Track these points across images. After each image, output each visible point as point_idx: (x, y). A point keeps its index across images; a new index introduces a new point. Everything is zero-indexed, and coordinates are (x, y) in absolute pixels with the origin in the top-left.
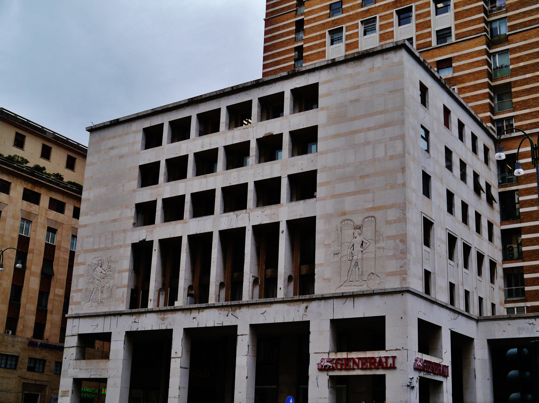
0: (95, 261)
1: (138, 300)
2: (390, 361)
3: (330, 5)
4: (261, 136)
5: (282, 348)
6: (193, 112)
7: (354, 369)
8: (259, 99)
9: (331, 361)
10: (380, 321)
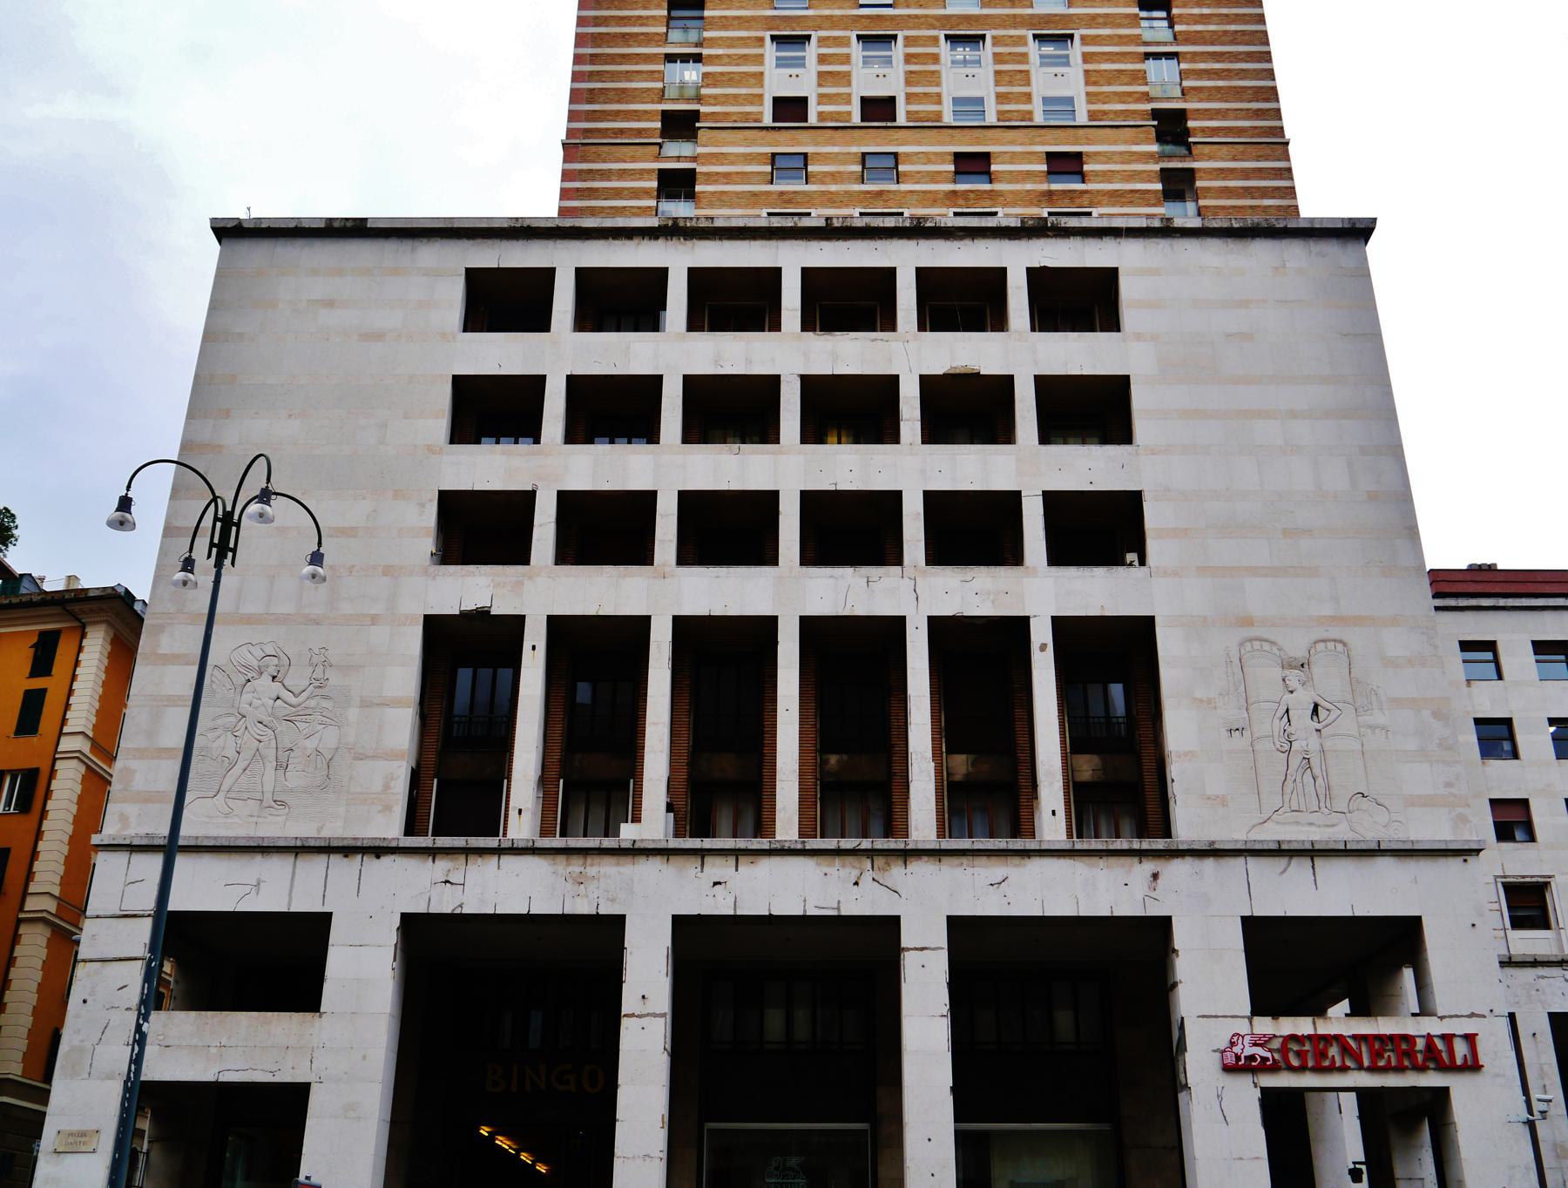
2: (1461, 1049)
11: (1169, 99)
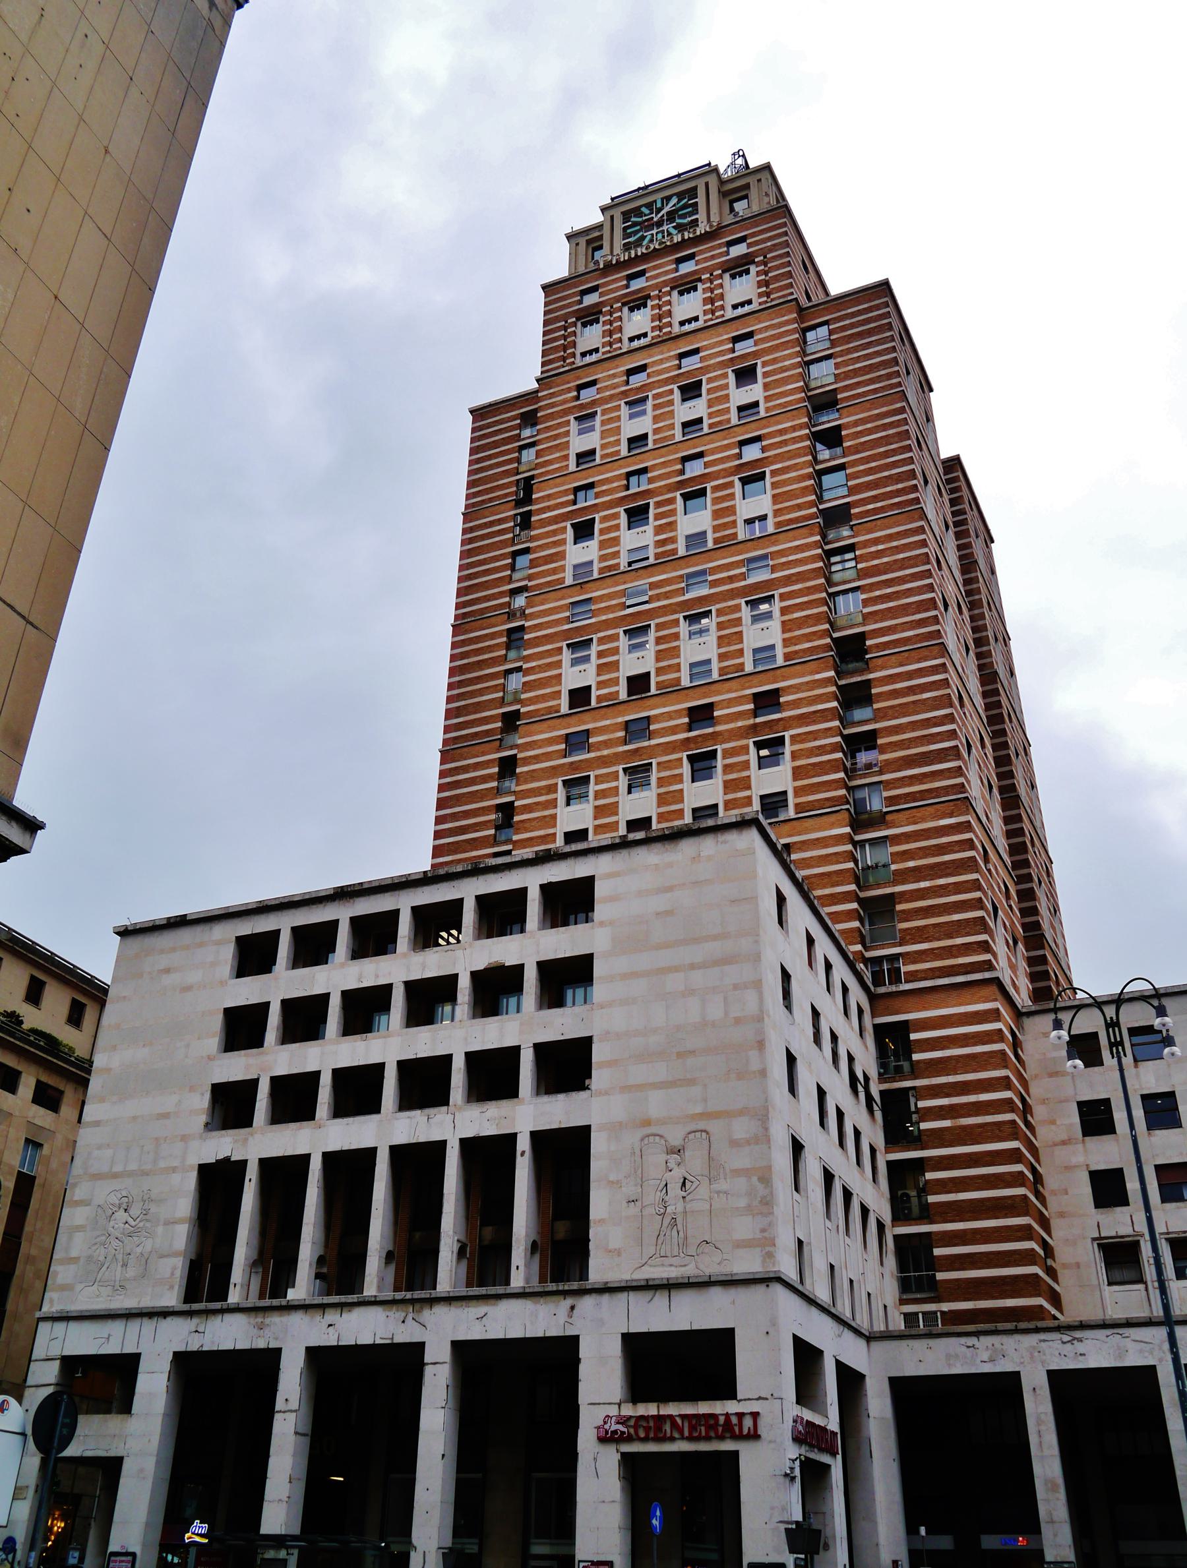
0: (114, 1199)
1: (205, 1284)
2: (748, 1423)
3: (567, 735)
4: (481, 967)
5: (521, 1393)
6: (343, 914)
7: (672, 1439)
8: (477, 897)
9: (623, 1420)
10: (724, 1339)
11: (852, 626)
